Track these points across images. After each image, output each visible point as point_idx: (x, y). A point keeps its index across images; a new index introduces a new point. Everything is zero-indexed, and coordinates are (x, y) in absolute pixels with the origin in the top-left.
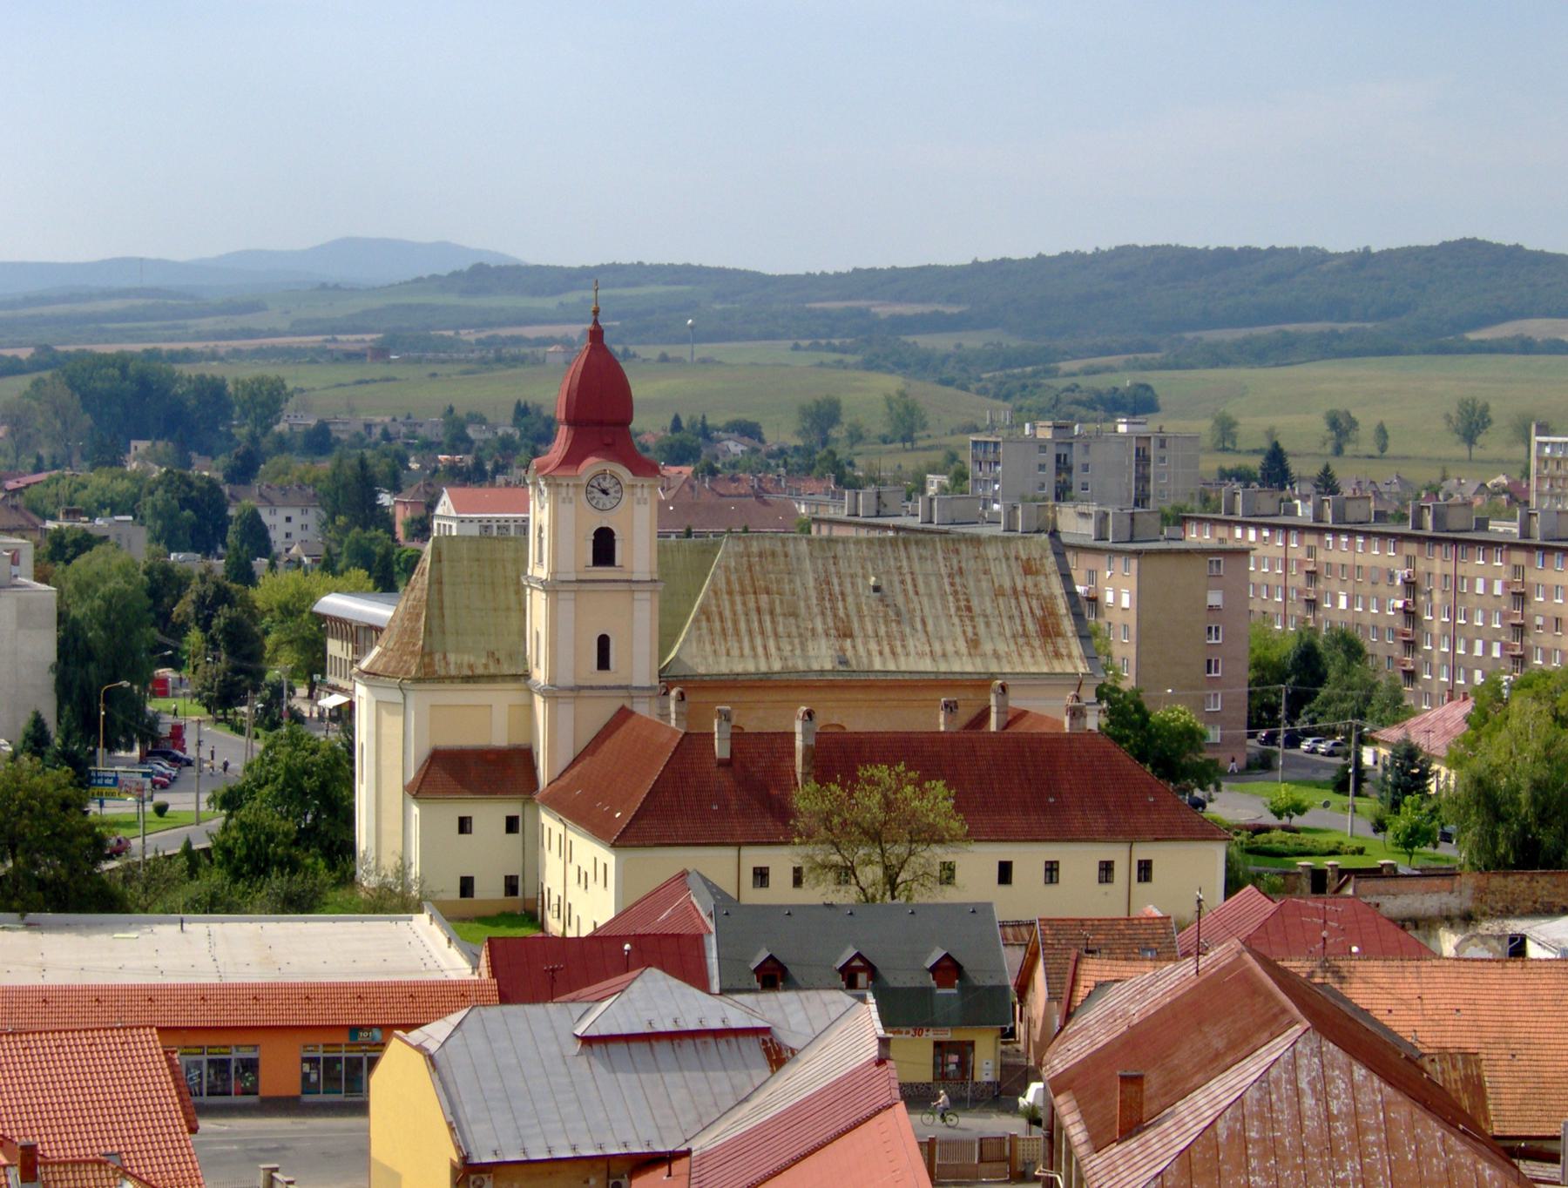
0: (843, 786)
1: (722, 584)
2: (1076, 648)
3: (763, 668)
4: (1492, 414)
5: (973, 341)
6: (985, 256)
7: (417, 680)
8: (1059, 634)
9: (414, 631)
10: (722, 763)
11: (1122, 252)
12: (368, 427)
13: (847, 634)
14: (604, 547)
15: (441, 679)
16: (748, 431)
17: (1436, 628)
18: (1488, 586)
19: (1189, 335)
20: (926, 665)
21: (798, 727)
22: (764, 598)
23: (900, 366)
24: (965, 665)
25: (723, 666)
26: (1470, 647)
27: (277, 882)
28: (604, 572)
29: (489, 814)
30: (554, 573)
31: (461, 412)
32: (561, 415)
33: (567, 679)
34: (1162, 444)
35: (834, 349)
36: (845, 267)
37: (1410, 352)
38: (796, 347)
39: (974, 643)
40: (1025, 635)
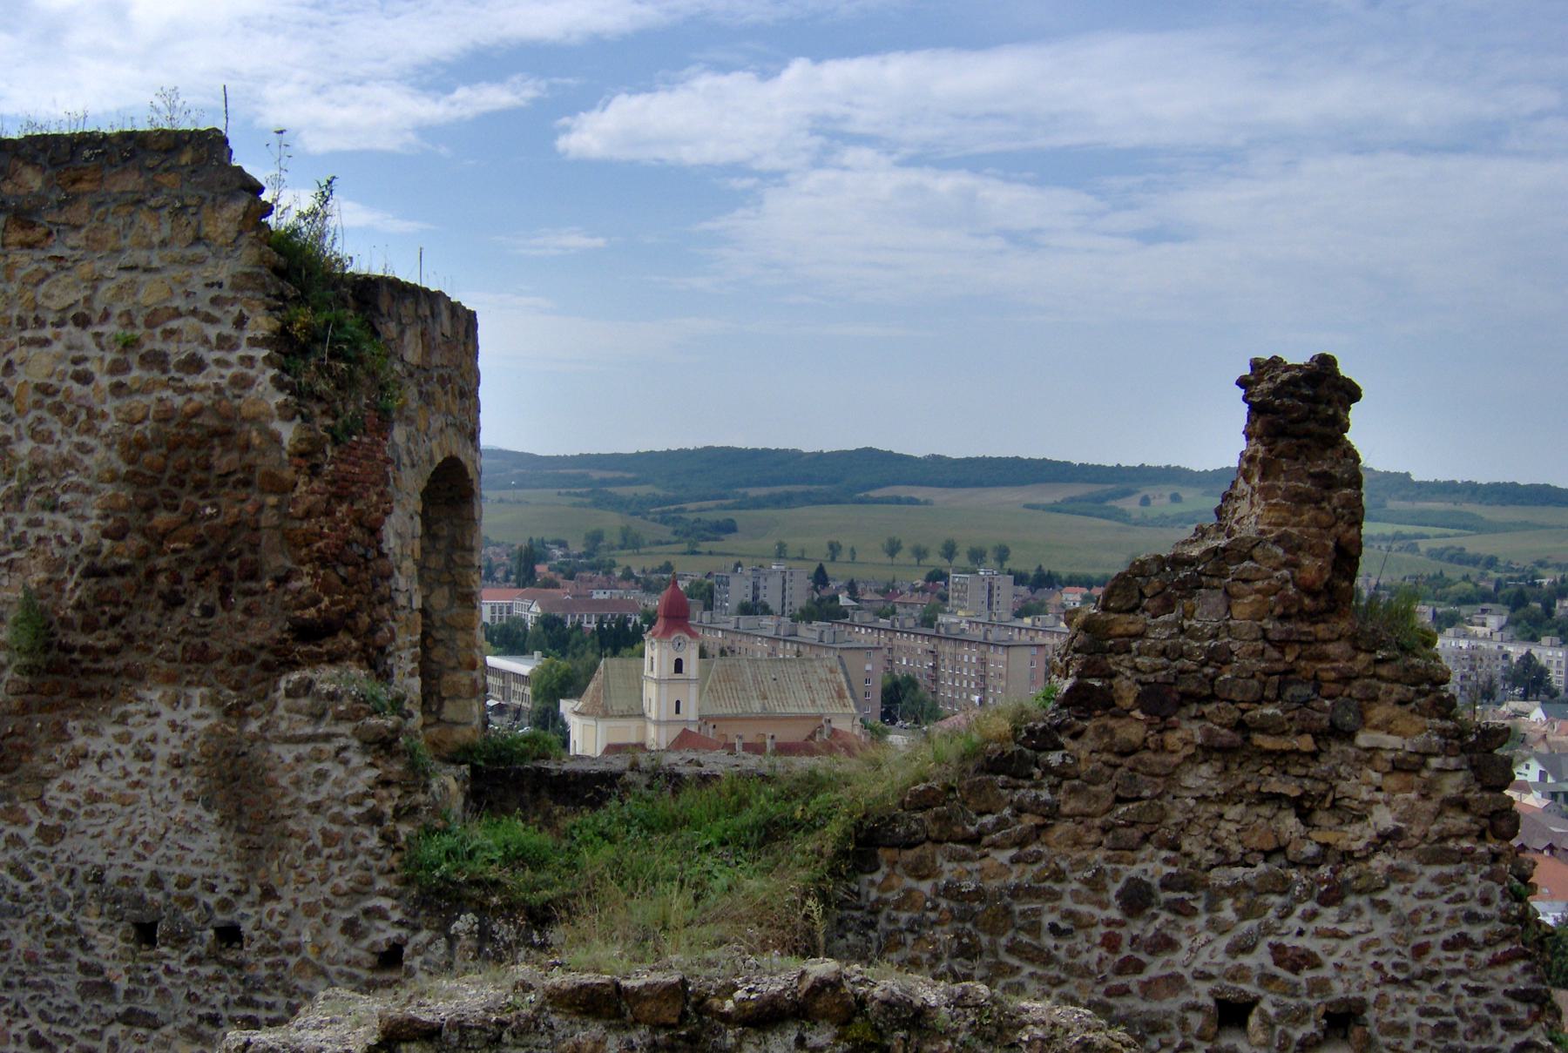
2: (851, 703)
4: (903, 544)
5: (643, 490)
11: (709, 450)
13: (765, 698)
16: (562, 544)
17: (946, 675)
18: (970, 659)
19: (742, 491)
20: (796, 710)
24: (811, 710)
26: (961, 683)
27: (1298, 953)
28: (678, 676)
32: (661, 613)
33: (663, 718)
37: (846, 503)
38: (559, 494)
39: (813, 702)
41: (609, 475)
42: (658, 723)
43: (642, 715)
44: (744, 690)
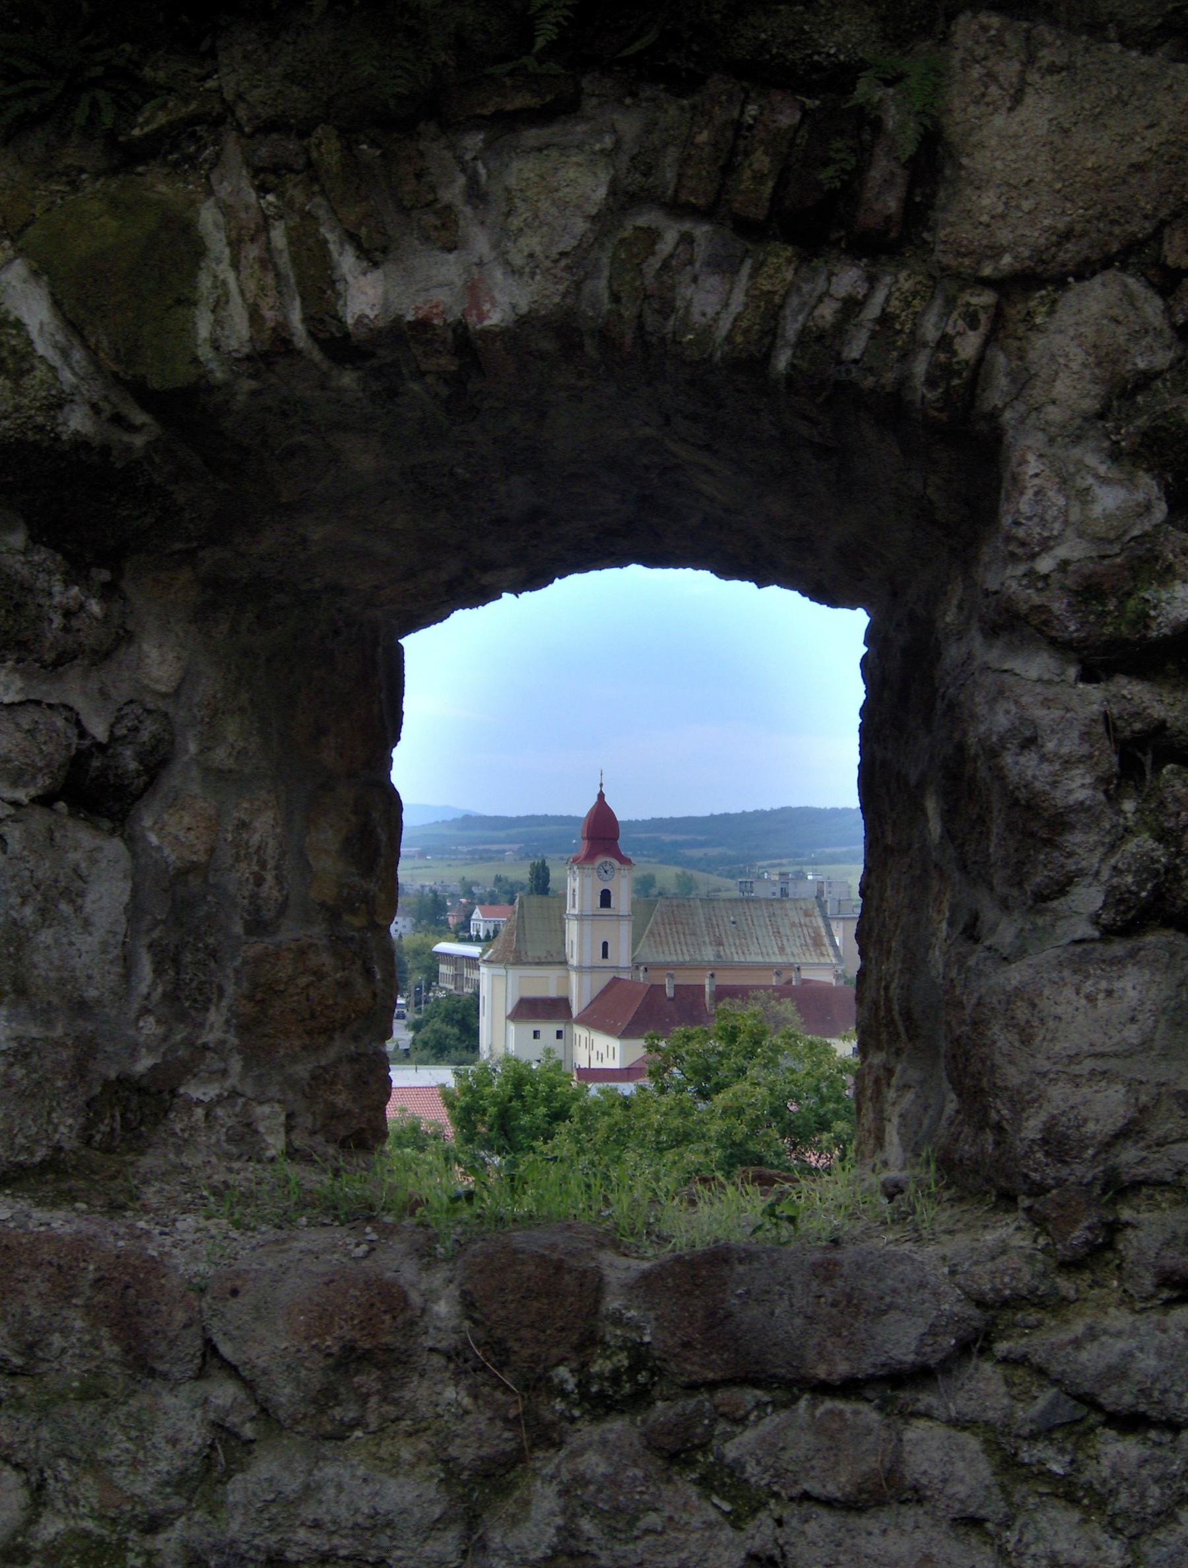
0: (742, 999)
1: (659, 919)
2: (831, 951)
3: (681, 959)
6: (717, 812)
7: (513, 964)
8: (824, 945)
9: (511, 941)
10: (670, 999)
12: (423, 887)
13: (720, 944)
14: (606, 899)
15: (524, 964)
20: (760, 959)
21: (707, 982)
22: (680, 927)
23: (677, 863)
24: (778, 959)
25: (661, 958)
28: (605, 911)
29: (548, 1030)
30: (581, 911)
31: (468, 879)
33: (587, 963)
34: (830, 884)
35: (645, 856)
36: (647, 817)
39: (782, 949)
40: (806, 945)
41: (680, 838)
42: (580, 969)
43: (564, 963)
44: (694, 934)
